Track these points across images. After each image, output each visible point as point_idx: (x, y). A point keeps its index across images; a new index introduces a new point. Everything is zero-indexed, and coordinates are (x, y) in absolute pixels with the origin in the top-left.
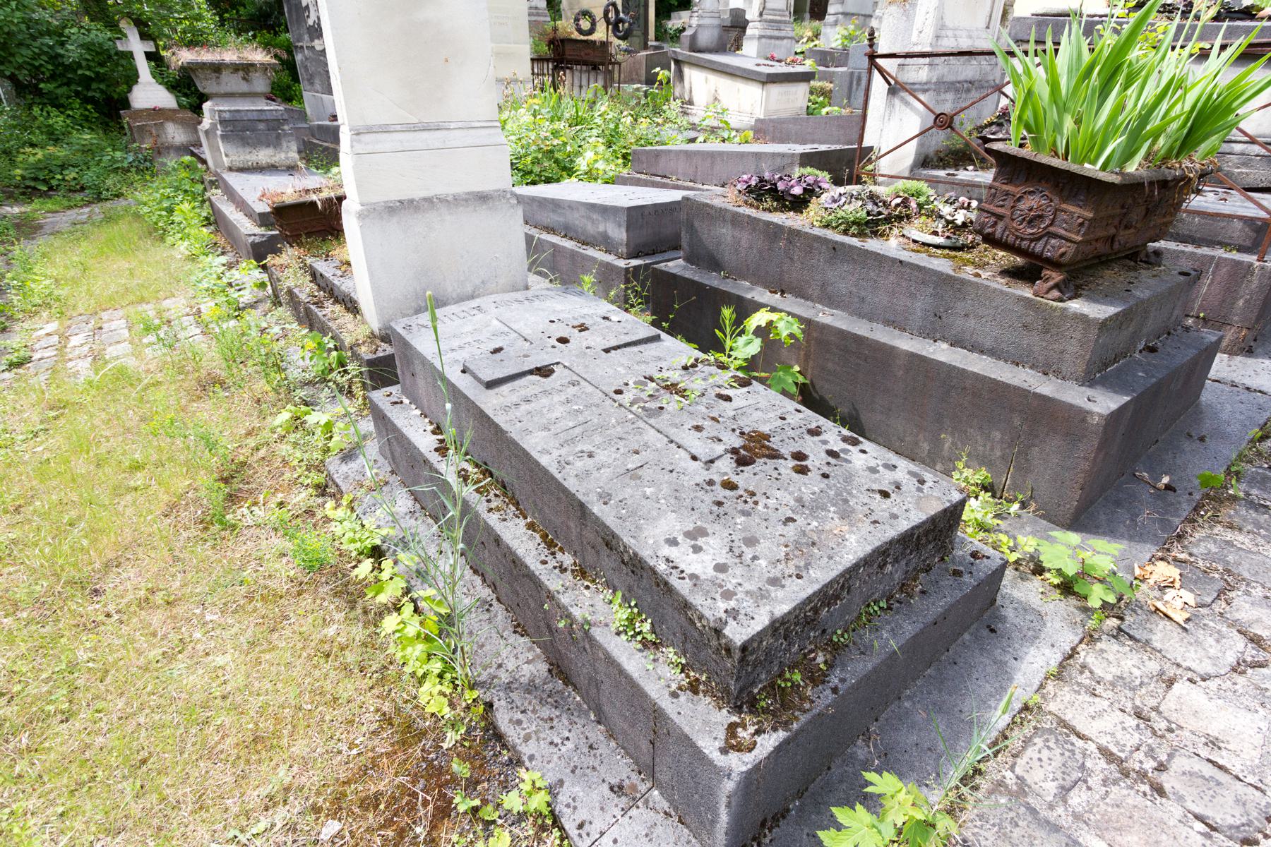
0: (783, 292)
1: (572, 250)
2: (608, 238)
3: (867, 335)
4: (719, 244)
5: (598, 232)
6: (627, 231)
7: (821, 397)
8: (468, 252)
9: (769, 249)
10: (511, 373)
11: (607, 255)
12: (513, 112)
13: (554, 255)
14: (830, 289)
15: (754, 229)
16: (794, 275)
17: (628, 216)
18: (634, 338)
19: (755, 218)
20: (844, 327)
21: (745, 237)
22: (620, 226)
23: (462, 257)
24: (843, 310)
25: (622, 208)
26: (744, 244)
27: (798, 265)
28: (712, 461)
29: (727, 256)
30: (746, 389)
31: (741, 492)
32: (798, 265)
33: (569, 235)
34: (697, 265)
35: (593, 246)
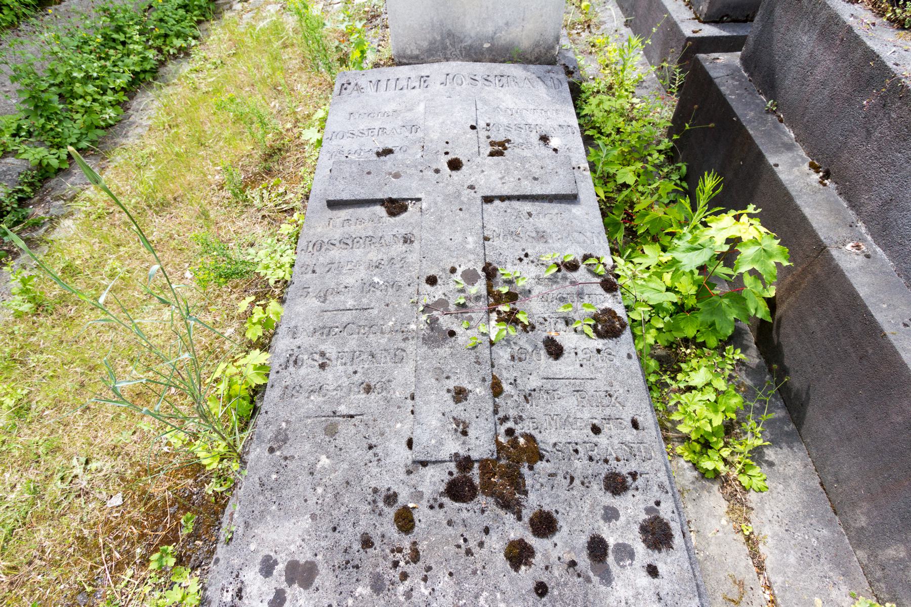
0: (827, 175)
3: (888, 329)
4: (788, 57)
7: (779, 344)
9: (847, 100)
10: (358, 198)
14: (894, 214)
15: (844, 56)
16: (857, 160)
18: (538, 190)
19: (857, 37)
20: (863, 292)
21: (826, 61)
24: (892, 258)
26: (819, 73)
27: (872, 147)
28: (424, 464)
29: (789, 82)
30: (600, 343)
31: (406, 542)
32: (872, 147)
34: (751, 75)
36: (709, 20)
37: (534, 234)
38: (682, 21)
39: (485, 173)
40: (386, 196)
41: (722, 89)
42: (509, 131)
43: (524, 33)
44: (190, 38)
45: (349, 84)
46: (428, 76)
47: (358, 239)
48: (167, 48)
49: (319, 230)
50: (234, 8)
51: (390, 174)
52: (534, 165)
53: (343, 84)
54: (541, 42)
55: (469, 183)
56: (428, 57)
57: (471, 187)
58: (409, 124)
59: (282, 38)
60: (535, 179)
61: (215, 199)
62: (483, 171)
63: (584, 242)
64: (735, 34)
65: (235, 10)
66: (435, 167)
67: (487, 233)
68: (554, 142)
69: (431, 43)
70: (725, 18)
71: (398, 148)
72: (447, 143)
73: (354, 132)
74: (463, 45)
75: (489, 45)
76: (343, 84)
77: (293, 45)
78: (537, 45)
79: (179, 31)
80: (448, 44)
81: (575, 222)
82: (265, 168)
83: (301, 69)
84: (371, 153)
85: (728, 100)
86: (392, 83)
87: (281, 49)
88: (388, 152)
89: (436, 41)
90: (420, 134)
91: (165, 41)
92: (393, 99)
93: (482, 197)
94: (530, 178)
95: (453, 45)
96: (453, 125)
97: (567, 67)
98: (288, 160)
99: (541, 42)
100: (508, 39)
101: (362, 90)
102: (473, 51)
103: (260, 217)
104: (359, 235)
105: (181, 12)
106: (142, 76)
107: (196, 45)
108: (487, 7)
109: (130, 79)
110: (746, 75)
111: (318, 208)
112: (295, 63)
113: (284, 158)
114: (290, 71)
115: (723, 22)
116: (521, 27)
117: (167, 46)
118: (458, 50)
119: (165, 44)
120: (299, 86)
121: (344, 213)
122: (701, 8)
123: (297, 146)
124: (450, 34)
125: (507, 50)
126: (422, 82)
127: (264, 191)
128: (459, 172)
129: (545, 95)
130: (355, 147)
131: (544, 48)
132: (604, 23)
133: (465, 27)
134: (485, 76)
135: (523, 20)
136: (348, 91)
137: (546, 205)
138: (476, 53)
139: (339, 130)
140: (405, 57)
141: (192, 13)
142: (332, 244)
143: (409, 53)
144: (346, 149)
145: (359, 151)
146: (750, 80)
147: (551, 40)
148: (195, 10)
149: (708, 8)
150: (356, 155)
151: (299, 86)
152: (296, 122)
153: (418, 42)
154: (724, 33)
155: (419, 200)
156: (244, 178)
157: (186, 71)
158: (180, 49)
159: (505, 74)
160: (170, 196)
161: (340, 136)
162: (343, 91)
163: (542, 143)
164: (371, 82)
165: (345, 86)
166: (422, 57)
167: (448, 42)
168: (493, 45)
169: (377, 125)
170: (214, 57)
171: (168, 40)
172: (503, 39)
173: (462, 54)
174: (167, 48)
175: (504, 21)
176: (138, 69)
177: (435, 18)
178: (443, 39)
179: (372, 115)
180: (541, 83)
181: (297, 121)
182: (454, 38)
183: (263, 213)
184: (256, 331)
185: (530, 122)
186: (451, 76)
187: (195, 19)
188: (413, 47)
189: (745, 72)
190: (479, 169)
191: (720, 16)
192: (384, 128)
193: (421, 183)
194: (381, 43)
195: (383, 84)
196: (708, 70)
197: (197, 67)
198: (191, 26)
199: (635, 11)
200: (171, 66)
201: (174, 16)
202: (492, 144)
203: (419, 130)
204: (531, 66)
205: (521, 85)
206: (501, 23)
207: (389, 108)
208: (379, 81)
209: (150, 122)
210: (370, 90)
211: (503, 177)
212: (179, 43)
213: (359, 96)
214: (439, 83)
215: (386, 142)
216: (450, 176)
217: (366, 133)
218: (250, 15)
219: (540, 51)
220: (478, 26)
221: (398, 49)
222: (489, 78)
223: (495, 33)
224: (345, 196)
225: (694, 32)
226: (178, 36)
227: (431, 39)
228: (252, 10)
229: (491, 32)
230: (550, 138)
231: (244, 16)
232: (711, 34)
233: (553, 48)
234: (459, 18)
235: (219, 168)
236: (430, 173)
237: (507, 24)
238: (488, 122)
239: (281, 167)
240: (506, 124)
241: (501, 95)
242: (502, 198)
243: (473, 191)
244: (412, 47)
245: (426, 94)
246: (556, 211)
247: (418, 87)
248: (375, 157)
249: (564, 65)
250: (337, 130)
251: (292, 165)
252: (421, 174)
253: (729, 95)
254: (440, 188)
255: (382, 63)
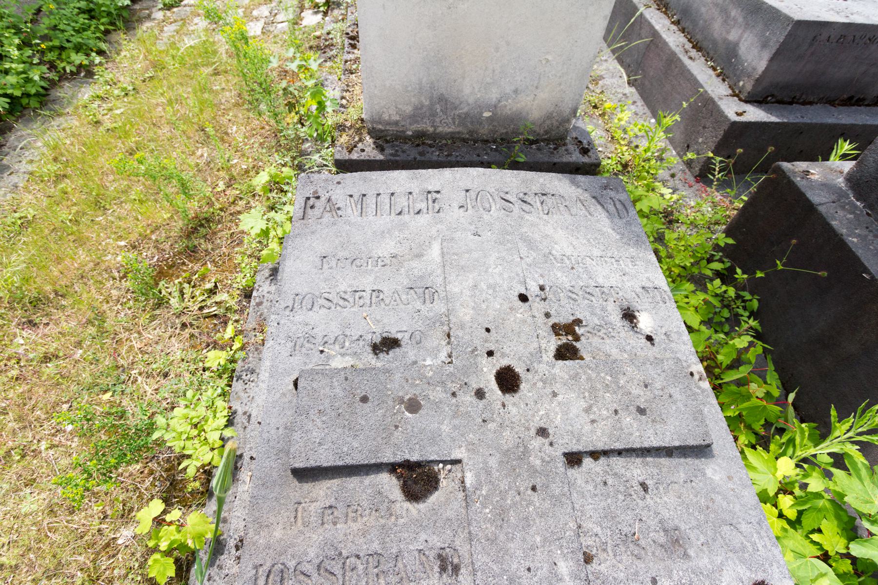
1: (674, 54)
2: (736, 56)
5: (725, 40)
6: (771, 60)
8: (508, 44)
11: (717, 81)
12: (659, 163)
13: (648, 46)
17: (789, 35)
22: (764, 46)
23: (497, 50)
25: (788, 18)
33: (683, 24)
34: (869, 206)
35: (708, 56)
36: (756, 99)
37: (662, 538)
38: (721, 99)
39: (560, 398)
40: (399, 458)
41: (834, 223)
42: (575, 300)
43: (536, 102)
44: (94, 54)
45: (318, 198)
46: (438, 192)
47: (353, 560)
48: (62, 65)
49: (278, 534)
50: (153, 16)
51: (401, 401)
52: (632, 379)
53: (308, 198)
54: (554, 114)
55: (537, 423)
56: (410, 124)
57: (542, 432)
58: (419, 284)
59: (214, 63)
60: (641, 411)
61: (115, 293)
62: (555, 395)
63: (743, 549)
64: (786, 121)
65: (154, 19)
66: (475, 386)
67: (587, 541)
68: (645, 322)
69: (416, 108)
70: (769, 98)
71: (407, 335)
72: (488, 330)
73: (330, 297)
74: (457, 112)
75: (490, 114)
76: (308, 198)
77: (226, 72)
78: (549, 116)
79: (79, 43)
80: (438, 110)
81: (718, 498)
82: (187, 247)
83: (237, 105)
84: (361, 343)
85: (850, 244)
86: (385, 199)
87: (212, 75)
88: (388, 344)
89: (422, 106)
90: (439, 307)
91: (60, 54)
92: (389, 232)
93: (565, 455)
94: (633, 409)
95: (445, 111)
96: (491, 291)
97: (580, 142)
98: (219, 235)
99: (554, 114)
100: (514, 109)
101: (340, 213)
102: (469, 120)
103: (179, 326)
104: (353, 549)
105: (82, 19)
106: (25, 101)
107: (101, 64)
108: (494, 71)
109: (7, 106)
110: (858, 203)
111: (275, 474)
112: (229, 96)
113: (215, 233)
114: (223, 107)
115: (767, 103)
116: (532, 96)
117: (62, 61)
118: (450, 118)
119: (59, 58)
120: (234, 128)
121: (324, 490)
122: (741, 83)
123: (231, 214)
124: (442, 99)
125: (512, 120)
126: (430, 202)
127: (186, 285)
128: (517, 396)
129: (610, 231)
130: (334, 330)
131: (557, 121)
132: (601, 78)
133: (462, 92)
134: (521, 195)
135: (537, 88)
136: (317, 212)
137: (664, 461)
138: (472, 123)
139: (306, 290)
140: (380, 123)
141: (99, 20)
142: (303, 573)
143: (387, 118)
144: (319, 332)
145: (341, 338)
146: (868, 214)
147: (567, 111)
148: (103, 17)
149: (754, 86)
150: (337, 347)
151: (234, 128)
152: (230, 180)
153: (399, 106)
154: (773, 119)
155: (457, 462)
156: (158, 260)
157: (86, 97)
158: (80, 66)
159: (547, 190)
160: (48, 288)
161: (307, 303)
162: (309, 211)
163: (626, 323)
164: (351, 196)
165: (311, 202)
166: (403, 123)
167: (438, 108)
168: (494, 114)
169: (367, 283)
170: (125, 82)
171: (64, 53)
172: (508, 107)
173: (454, 123)
174: (62, 65)
175: (513, 88)
176: (17, 93)
177: (424, 80)
178: (432, 104)
179: (358, 262)
180: (599, 207)
181: (232, 178)
182: (446, 104)
183: (184, 319)
184: (165, 569)
185: (601, 281)
186: (472, 194)
187: (102, 28)
188: (392, 111)
189: (857, 200)
190: (548, 390)
191: (764, 96)
192: (379, 291)
193: (456, 422)
194: (345, 94)
195: (371, 201)
196: (803, 190)
197: (101, 93)
198: (98, 38)
199: (643, 70)
200: (65, 91)
201: (73, 24)
202: (556, 329)
203: (436, 297)
204: (580, 178)
205: (574, 211)
206: (509, 89)
207: (386, 248)
208: (364, 195)
209: (30, 168)
210: (351, 212)
211: (590, 407)
212: (78, 58)
213: (334, 224)
214: (455, 205)
215: (385, 321)
216: (504, 406)
217: (351, 300)
218: (174, 27)
219: (552, 124)
220: (479, 91)
221: (372, 113)
222: (526, 198)
223: (499, 101)
224: (326, 459)
225: (738, 114)
226: (78, 48)
227: (417, 103)
228: (175, 21)
229: (494, 100)
230: (637, 314)
231: (165, 29)
232: (759, 120)
233: (568, 121)
234: (455, 81)
235: (123, 243)
236: (468, 398)
237: (516, 91)
238: (541, 283)
239: (210, 247)
240: (567, 286)
241: (549, 230)
242: (595, 455)
243: (546, 441)
244: (391, 112)
245: (439, 226)
246: (682, 476)
247: (425, 211)
248: (369, 359)
249: (576, 138)
250: (303, 290)
251: (224, 242)
252: (454, 400)
253: (849, 236)
254: (491, 436)
255: (348, 124)
